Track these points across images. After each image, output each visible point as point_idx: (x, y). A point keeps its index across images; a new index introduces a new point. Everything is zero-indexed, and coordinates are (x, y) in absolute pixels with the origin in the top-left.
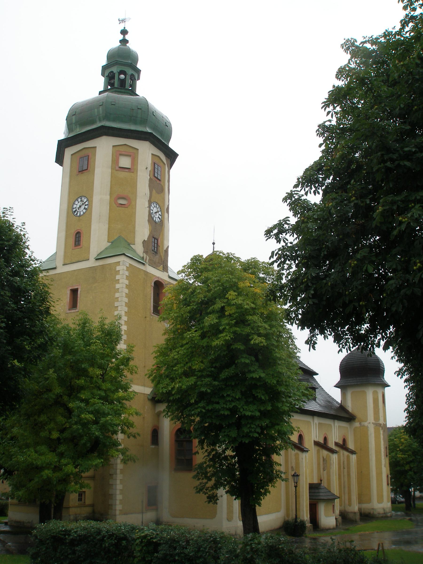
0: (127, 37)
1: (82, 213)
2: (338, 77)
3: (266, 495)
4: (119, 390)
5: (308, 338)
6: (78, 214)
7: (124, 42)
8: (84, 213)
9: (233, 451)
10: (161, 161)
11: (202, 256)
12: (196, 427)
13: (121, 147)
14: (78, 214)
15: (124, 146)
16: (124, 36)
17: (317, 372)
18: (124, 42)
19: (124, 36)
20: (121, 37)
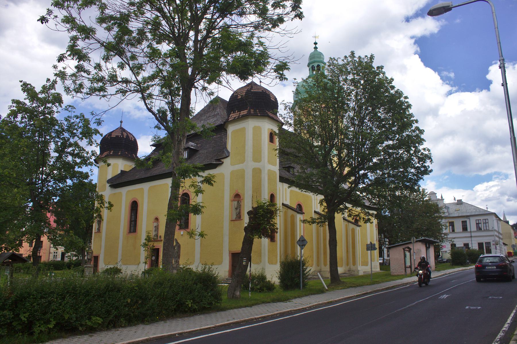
7: (316, 48)
18: (316, 48)
19: (315, 46)
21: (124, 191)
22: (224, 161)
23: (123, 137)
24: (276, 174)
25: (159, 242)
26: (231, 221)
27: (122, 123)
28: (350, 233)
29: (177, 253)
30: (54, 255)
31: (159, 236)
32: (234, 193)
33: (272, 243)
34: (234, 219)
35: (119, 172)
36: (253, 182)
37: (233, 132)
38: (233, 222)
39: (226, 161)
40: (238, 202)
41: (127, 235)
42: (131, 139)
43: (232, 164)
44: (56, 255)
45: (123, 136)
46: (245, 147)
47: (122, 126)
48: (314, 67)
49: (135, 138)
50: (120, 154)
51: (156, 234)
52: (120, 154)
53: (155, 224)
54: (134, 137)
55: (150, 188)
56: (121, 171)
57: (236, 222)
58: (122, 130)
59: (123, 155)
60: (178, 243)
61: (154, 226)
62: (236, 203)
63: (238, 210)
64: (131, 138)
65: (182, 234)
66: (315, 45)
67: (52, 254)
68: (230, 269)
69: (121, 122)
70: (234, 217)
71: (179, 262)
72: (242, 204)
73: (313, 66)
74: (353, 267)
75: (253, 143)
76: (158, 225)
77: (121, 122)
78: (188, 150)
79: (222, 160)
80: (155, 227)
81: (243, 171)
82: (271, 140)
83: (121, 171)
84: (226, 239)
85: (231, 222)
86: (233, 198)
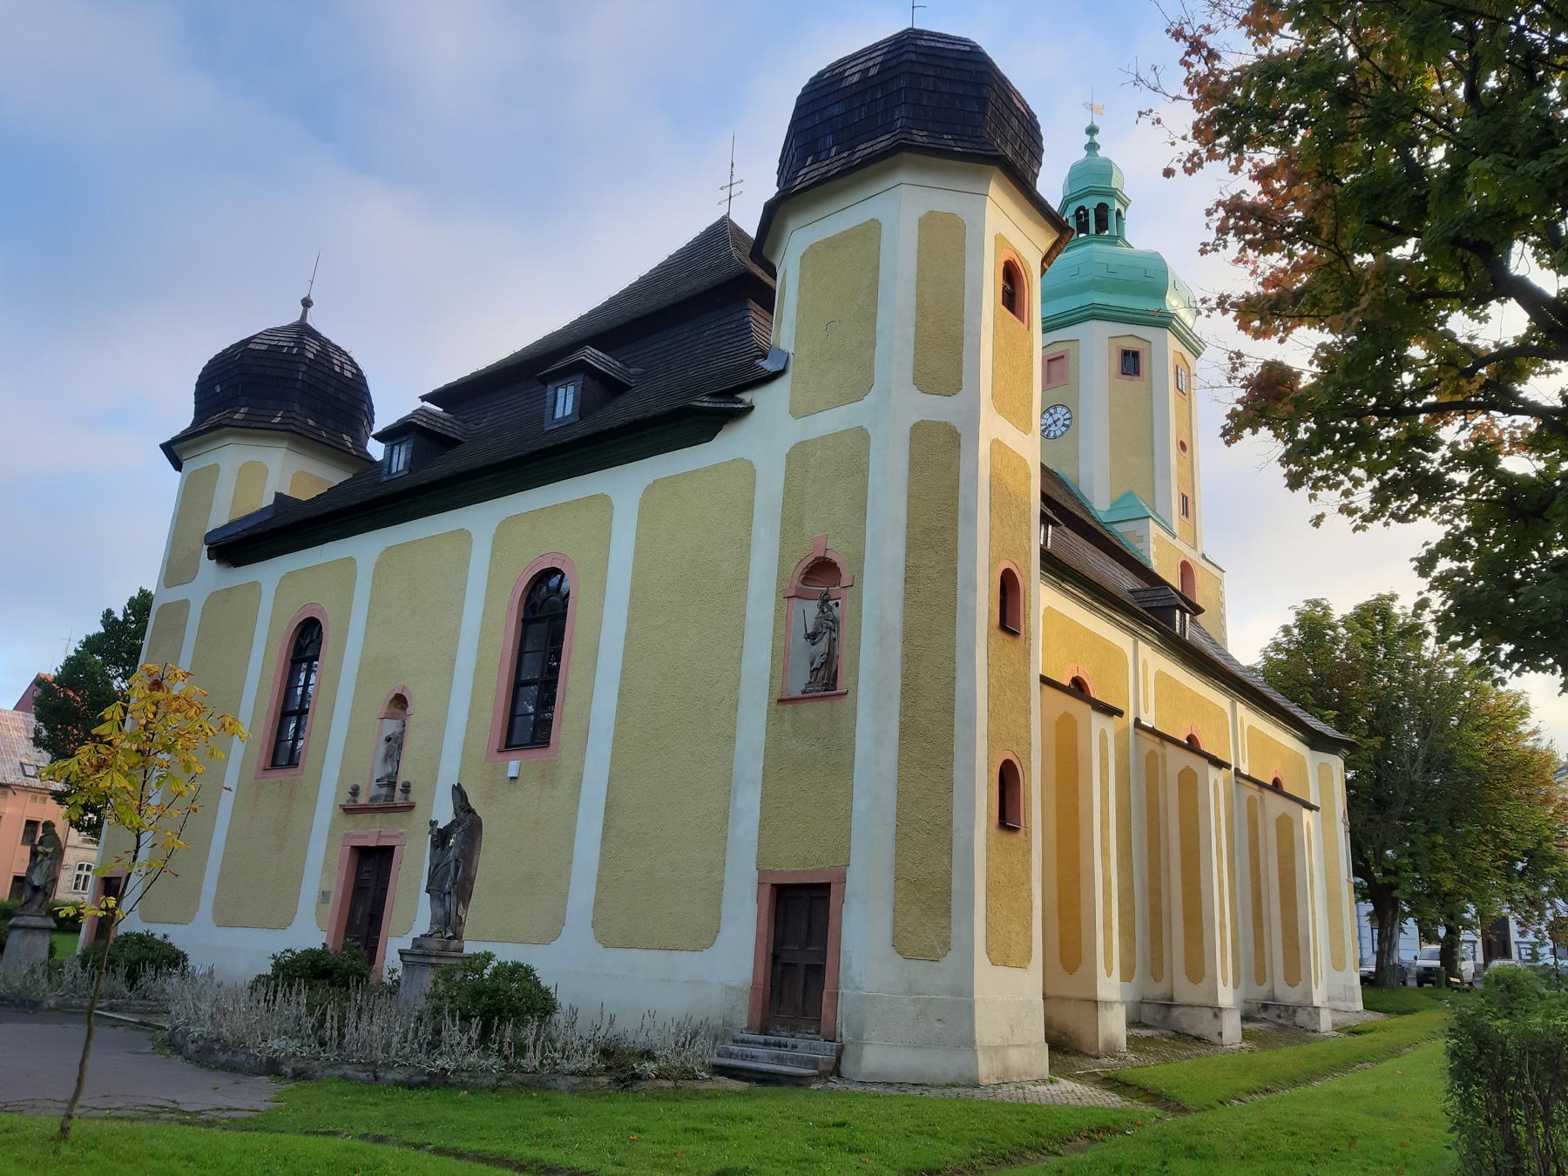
0: (1096, 138)
1: (1058, 433)
2: (1249, 38)
3: (1424, 517)
4: (1470, 523)
5: (648, 1055)
6: (1052, 435)
7: (1092, 147)
8: (1063, 433)
9: (1452, 481)
10: (1138, 341)
11: (1415, 569)
12: (1501, 446)
13: (1124, 339)
14: (1052, 435)
15: (1131, 338)
16: (1092, 138)
17: (1386, 592)
18: (1092, 147)
19: (1092, 138)
20: (1087, 139)
21: (270, 574)
22: (759, 398)
23: (301, 354)
24: (1028, 477)
25: (395, 816)
26: (780, 701)
27: (309, 310)
28: (1270, 836)
29: (457, 869)
30: (78, 877)
31: (399, 786)
32: (807, 552)
33: (1007, 837)
34: (798, 694)
35: (268, 500)
36: (910, 496)
37: (813, 254)
38: (789, 707)
39: (768, 402)
40: (825, 601)
41: (256, 778)
42: (337, 369)
43: (795, 413)
44: (87, 877)
45: (302, 349)
46: (874, 316)
47: (309, 321)
48: (1087, 214)
49: (358, 370)
50: (277, 420)
51: (389, 776)
52: (277, 420)
53: (391, 727)
54: (354, 365)
55: (385, 561)
56: (279, 497)
57: (810, 711)
58: (302, 331)
59: (292, 427)
60: (471, 811)
61: (386, 735)
62: (812, 608)
63: (822, 646)
64: (342, 368)
65: (512, 773)
66: (1088, 137)
67: (70, 873)
68: (761, 979)
69: (307, 303)
70: (799, 680)
71: (460, 922)
72: (843, 611)
73: (1082, 208)
74: (1185, 991)
75: (920, 295)
76: (402, 733)
77: (307, 303)
78: (580, 379)
79: (747, 397)
80: (388, 739)
81: (861, 437)
82: (1012, 297)
83: (279, 497)
84: (748, 803)
85: (781, 707)
86: (796, 582)
